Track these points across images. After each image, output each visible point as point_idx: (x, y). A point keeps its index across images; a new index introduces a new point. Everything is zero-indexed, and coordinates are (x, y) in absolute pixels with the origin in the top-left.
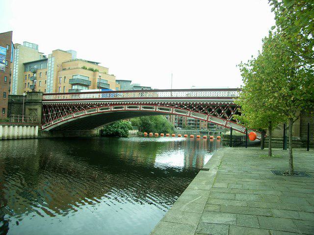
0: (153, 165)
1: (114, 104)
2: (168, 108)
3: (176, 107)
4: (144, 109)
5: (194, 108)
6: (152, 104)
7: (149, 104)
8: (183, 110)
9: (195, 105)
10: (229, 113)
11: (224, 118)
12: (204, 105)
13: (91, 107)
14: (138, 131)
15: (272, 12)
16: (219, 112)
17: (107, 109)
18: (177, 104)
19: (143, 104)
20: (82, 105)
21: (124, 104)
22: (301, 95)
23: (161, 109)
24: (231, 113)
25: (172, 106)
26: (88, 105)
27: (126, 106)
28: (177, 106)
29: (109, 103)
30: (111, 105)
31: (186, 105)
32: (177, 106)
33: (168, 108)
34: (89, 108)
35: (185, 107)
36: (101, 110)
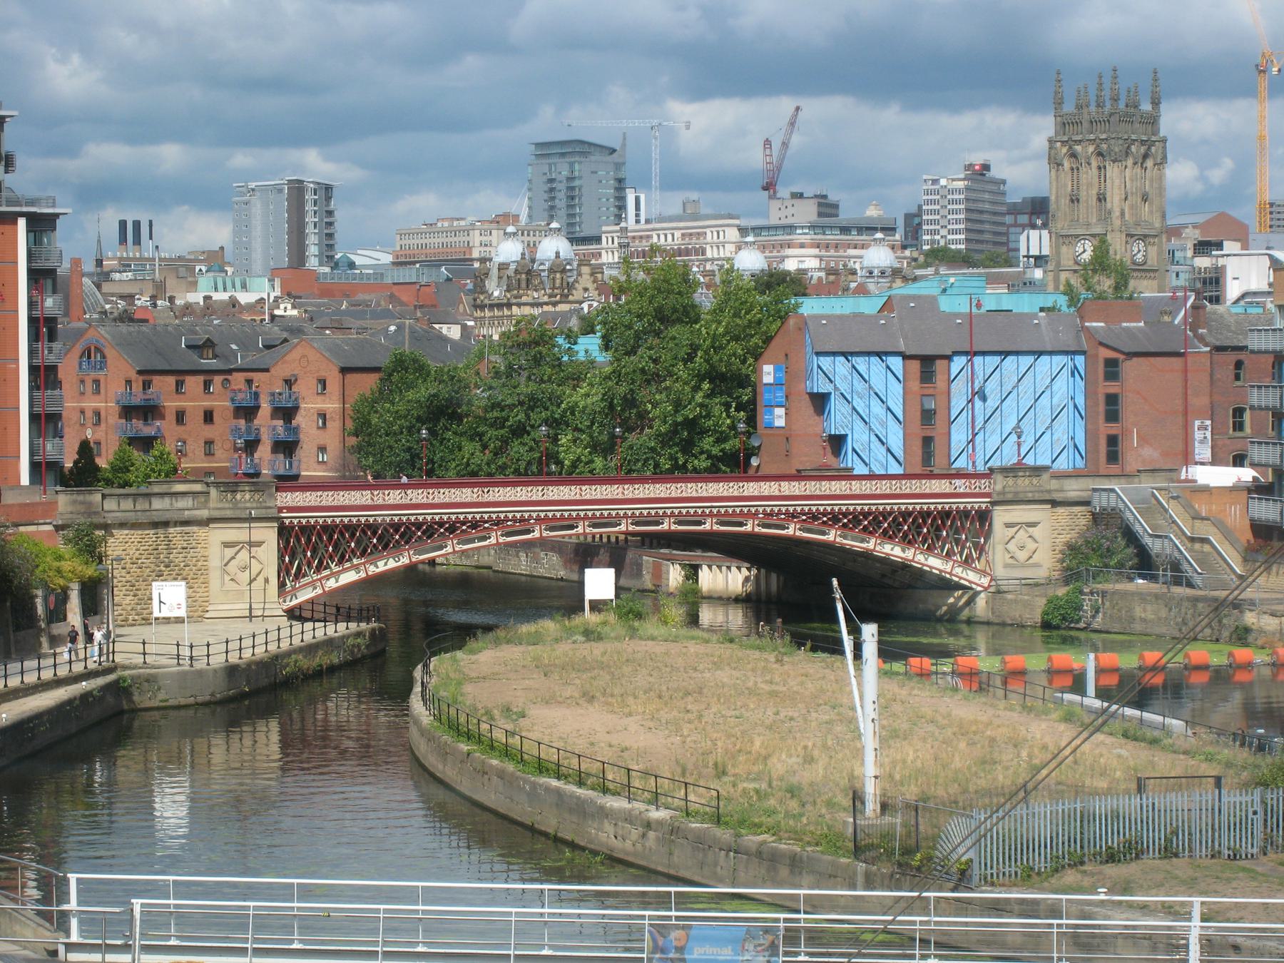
9: (845, 515)
23: (765, 526)
26: (463, 523)
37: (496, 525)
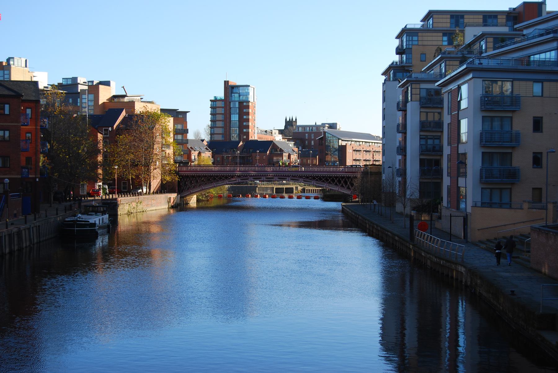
0: (555, 61)
2: (298, 179)
3: (304, 178)
4: (242, 181)
5: (317, 179)
6: (286, 176)
7: (283, 176)
8: (309, 180)
9: (317, 177)
10: (339, 182)
11: (336, 184)
12: (323, 177)
14: (398, 167)
15: (382, 74)
16: (346, 183)
18: (311, 177)
19: (279, 176)
20: (223, 176)
21: (263, 176)
22: (67, 335)
24: (341, 182)
26: (229, 176)
27: (252, 178)
28: (304, 177)
31: (310, 177)
32: (304, 177)
33: (298, 179)
34: (230, 179)
35: (310, 178)
36: (242, 180)
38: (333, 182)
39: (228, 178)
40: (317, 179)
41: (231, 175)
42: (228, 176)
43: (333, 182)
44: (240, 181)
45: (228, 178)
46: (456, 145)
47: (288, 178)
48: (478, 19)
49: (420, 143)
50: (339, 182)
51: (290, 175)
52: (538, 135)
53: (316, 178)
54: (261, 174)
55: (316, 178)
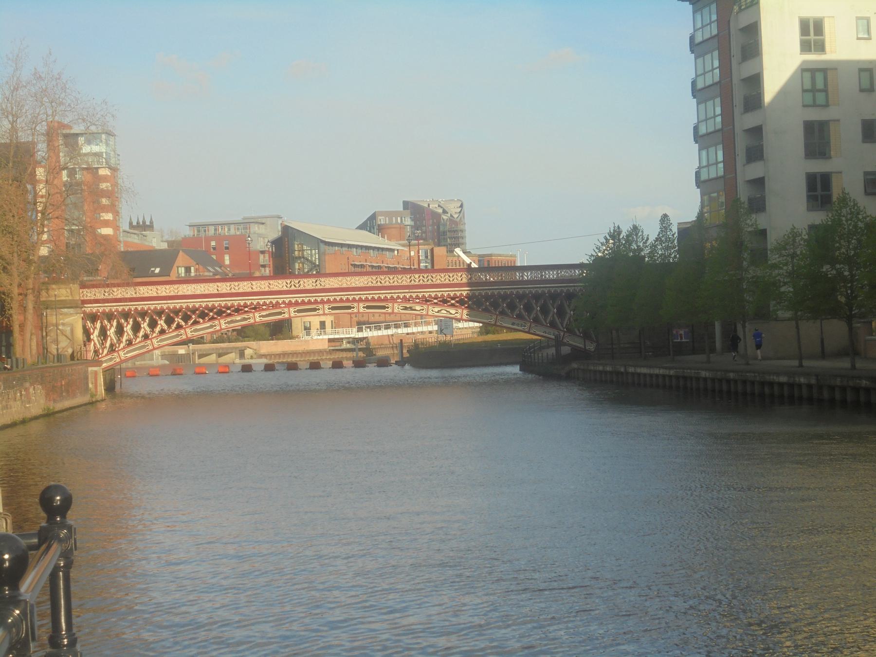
1: (297, 304)
3: (435, 303)
10: (512, 307)
13: (215, 313)
17: (280, 313)
25: (427, 301)
26: (229, 308)
28: (435, 301)
29: (284, 302)
30: (290, 304)
31: (453, 299)
32: (435, 301)
34: (230, 315)
37: (255, 308)
38: (495, 309)
39: (224, 312)
40: (211, 314)
41: (233, 306)
42: (223, 308)
43: (495, 309)
44: (362, 310)
45: (224, 312)
46: (732, 127)
47: (390, 305)
48: (84, 407)
49: (694, 27)
50: (512, 307)
51: (398, 297)
52: (811, 12)
53: (207, 315)
54: (546, 287)
55: (207, 315)
